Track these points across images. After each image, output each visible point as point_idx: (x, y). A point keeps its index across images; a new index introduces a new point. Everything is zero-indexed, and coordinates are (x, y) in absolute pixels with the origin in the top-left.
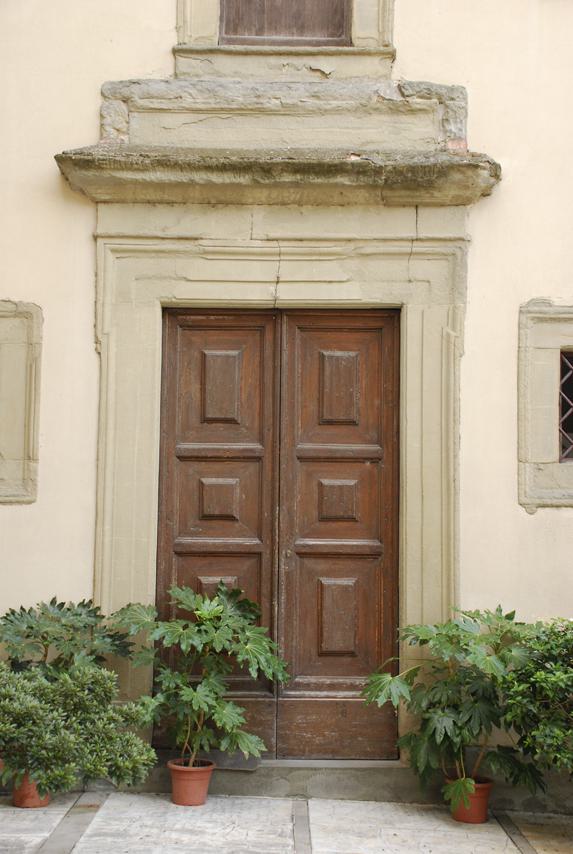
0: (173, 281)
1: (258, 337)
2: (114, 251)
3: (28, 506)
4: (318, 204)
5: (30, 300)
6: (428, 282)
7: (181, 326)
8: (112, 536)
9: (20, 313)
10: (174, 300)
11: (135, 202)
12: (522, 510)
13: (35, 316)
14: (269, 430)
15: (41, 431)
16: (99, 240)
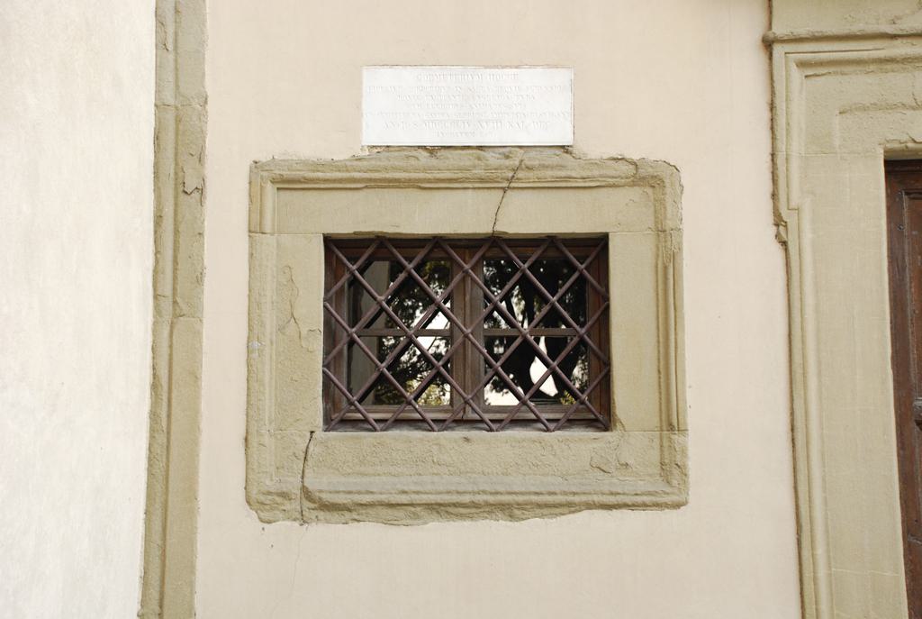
0: (909, 113)
2: (802, 64)
3: (674, 512)
5: (660, 156)
7: (907, 194)
8: (830, 568)
10: (911, 145)
14: (913, 346)
16: (778, 50)
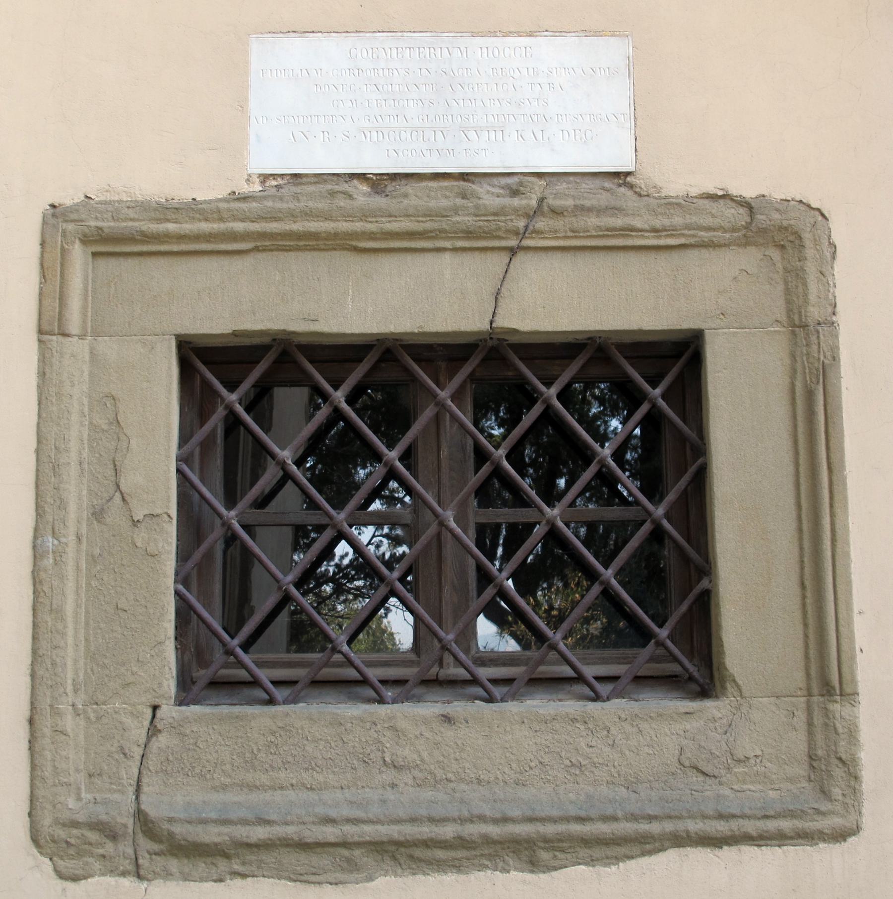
1: (257, 528)
4: (613, 521)
9: (763, 231)
11: (793, 357)
13: (807, 236)
15: (858, 603)
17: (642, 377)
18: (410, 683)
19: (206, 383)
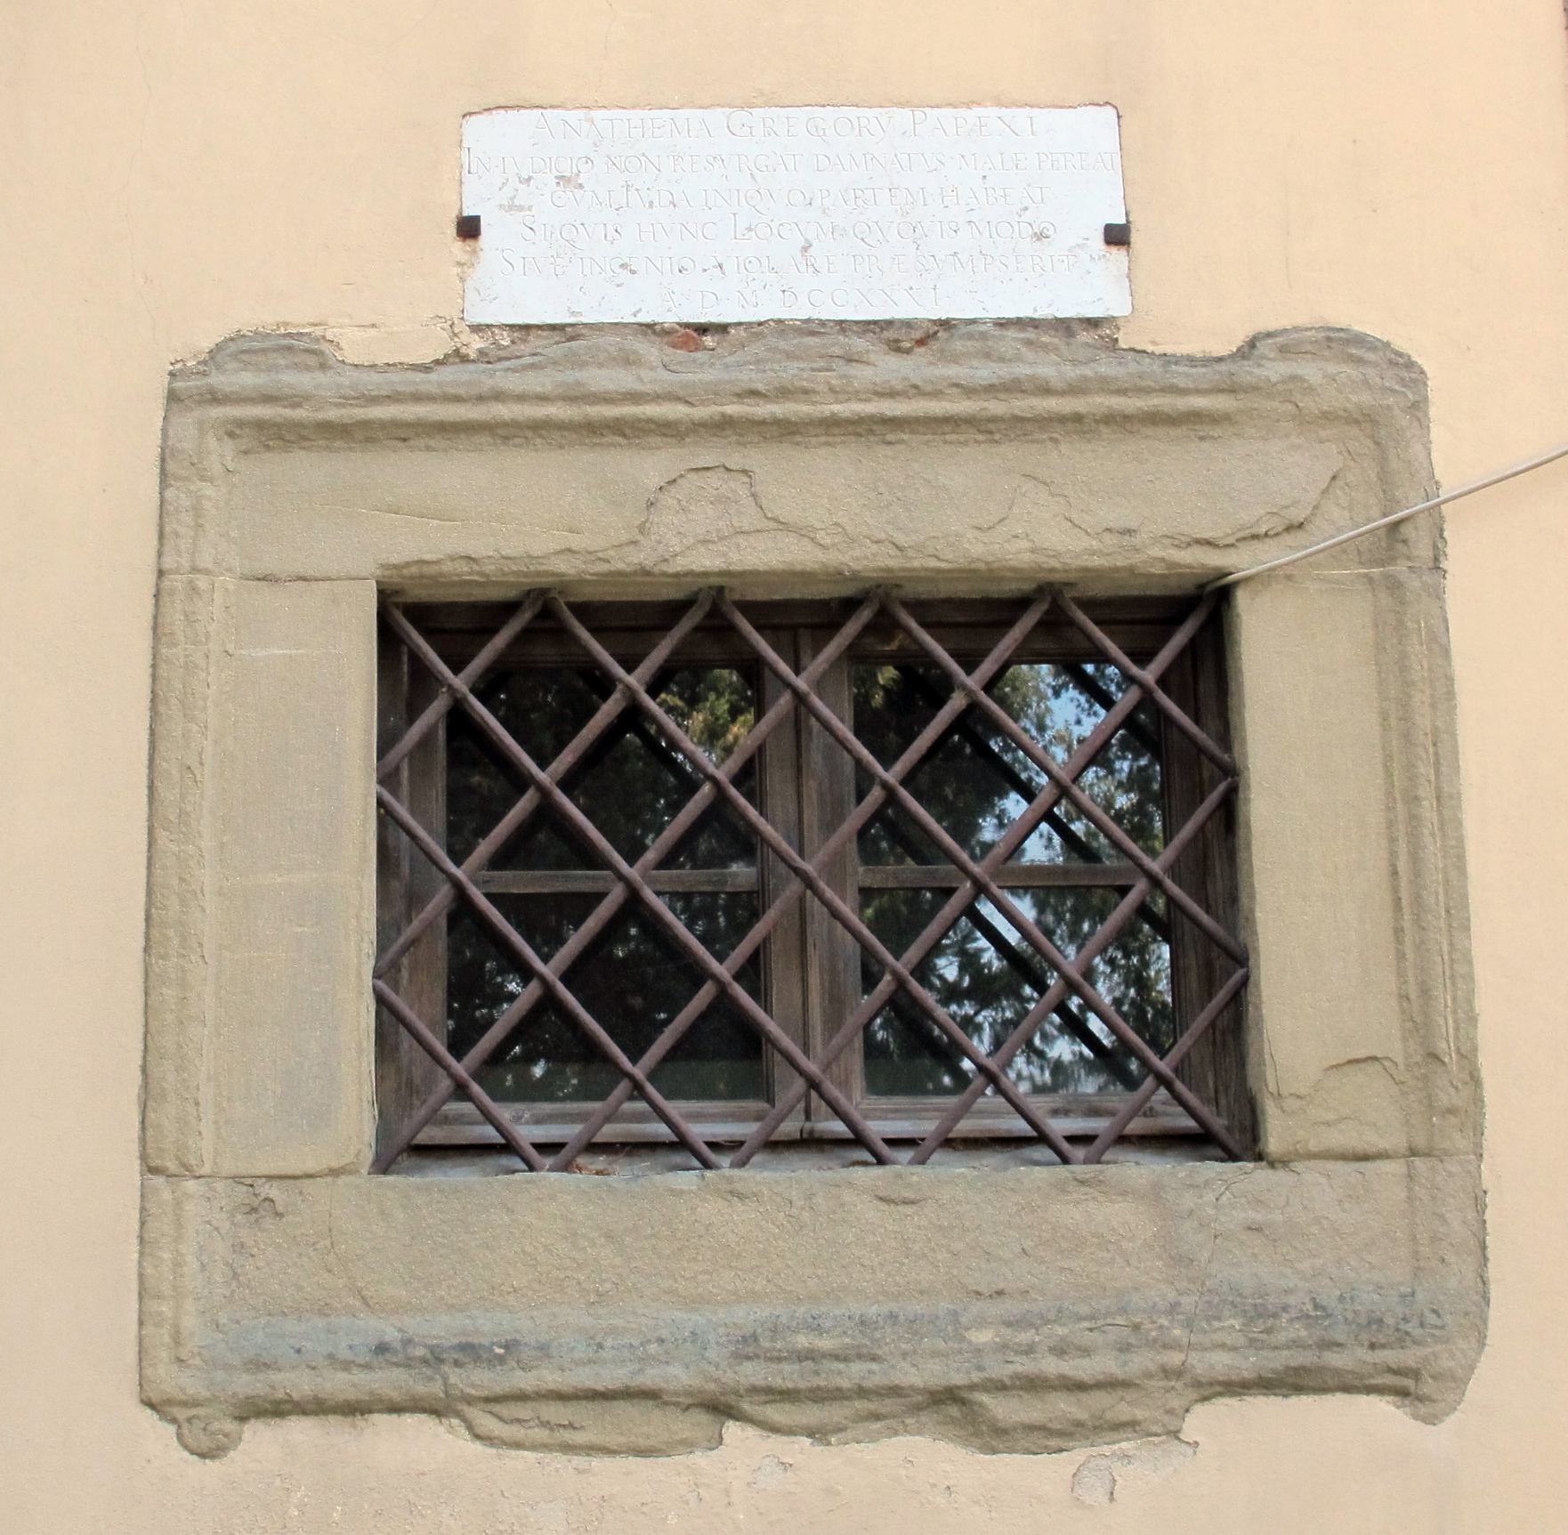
6: (744, 472)
12: (158, 1435)
17: (952, 656)
18: (1098, 1142)
19: (416, 660)
